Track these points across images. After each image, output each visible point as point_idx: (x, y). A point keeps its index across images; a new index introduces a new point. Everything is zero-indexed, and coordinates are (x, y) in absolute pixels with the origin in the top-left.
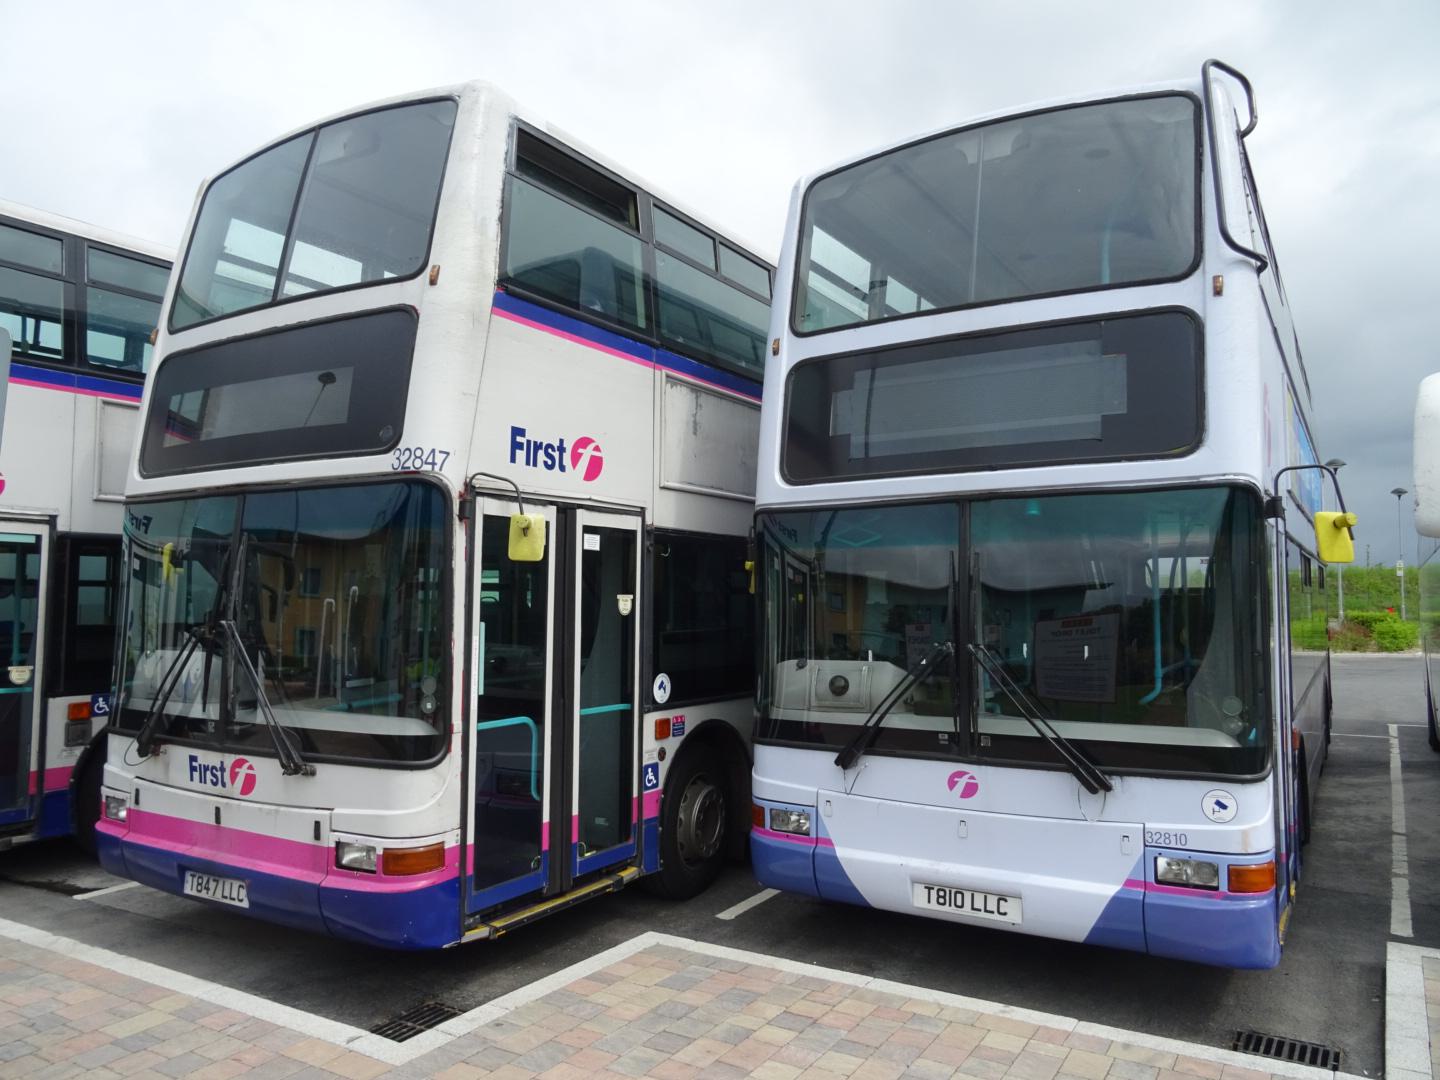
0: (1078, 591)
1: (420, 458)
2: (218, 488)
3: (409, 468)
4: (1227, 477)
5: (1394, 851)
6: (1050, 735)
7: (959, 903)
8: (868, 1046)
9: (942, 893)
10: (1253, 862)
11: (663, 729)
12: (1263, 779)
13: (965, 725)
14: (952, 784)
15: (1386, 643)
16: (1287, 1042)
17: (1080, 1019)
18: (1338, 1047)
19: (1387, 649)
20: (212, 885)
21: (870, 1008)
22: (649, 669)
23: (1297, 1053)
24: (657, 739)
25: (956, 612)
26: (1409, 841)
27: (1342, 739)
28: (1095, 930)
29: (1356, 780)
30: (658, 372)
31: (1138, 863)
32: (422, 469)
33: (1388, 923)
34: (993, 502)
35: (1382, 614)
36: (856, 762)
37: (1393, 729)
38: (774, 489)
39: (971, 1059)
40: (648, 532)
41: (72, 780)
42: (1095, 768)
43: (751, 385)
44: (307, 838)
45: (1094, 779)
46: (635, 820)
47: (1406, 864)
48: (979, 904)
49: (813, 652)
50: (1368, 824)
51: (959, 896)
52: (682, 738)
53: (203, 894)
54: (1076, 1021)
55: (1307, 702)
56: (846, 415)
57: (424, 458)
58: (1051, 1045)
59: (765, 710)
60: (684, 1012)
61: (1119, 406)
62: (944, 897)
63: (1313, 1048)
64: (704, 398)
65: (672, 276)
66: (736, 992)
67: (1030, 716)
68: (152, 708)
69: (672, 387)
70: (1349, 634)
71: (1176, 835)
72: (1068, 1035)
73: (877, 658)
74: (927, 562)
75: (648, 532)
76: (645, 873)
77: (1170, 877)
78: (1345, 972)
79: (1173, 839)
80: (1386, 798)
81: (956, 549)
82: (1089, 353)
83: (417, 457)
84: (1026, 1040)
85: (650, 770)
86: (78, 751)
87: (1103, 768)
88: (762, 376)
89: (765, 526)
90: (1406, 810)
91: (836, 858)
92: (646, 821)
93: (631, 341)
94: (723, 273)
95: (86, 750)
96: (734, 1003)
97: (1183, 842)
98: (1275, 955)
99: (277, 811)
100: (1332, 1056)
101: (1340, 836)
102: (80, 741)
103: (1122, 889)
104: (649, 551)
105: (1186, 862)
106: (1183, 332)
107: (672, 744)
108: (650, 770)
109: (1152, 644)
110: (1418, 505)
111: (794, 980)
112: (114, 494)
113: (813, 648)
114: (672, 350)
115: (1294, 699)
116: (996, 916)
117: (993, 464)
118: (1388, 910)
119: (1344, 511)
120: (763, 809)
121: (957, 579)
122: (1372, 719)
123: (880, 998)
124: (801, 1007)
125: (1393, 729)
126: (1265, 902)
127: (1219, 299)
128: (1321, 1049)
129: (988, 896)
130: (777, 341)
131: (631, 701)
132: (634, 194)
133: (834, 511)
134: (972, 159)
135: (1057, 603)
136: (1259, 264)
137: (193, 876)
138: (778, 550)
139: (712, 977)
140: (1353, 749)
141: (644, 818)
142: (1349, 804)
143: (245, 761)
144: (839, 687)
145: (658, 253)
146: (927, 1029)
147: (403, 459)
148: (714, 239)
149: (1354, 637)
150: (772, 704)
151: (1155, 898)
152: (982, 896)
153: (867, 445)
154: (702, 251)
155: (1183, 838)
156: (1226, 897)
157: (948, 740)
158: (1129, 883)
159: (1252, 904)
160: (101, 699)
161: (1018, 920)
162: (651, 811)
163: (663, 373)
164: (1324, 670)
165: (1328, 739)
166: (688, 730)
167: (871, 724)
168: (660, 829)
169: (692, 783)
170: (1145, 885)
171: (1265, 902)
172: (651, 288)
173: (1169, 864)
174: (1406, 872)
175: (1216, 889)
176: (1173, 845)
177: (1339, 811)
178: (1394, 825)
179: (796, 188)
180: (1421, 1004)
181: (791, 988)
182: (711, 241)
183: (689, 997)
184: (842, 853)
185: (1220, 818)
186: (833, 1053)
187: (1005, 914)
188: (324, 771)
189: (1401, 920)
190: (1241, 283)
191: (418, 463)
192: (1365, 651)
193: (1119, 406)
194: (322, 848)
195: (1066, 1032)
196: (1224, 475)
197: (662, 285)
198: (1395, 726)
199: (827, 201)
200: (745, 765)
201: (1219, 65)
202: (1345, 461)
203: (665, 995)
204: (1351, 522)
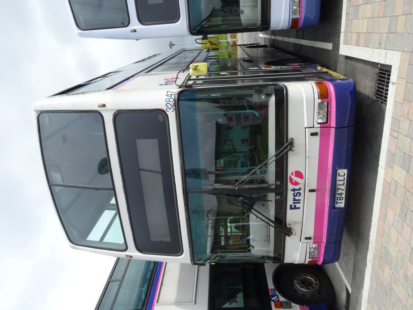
1: (169, 99)
2: (185, 205)
3: (173, 103)
10: (316, 90)
13: (271, 191)
20: (340, 192)
32: (174, 98)
41: (305, 306)
44: (317, 139)
53: (344, 196)
57: (169, 98)
59: (269, 258)
68: (273, 226)
83: (169, 101)
86: (293, 304)
95: (293, 302)
99: (308, 156)
102: (289, 304)
105: (319, 113)
112: (193, 299)
127: (106, 105)
137: (337, 203)
143: (290, 176)
147: (170, 107)
160: (272, 299)
167: (273, 225)
182: (110, 283)
187: (344, 174)
188: (291, 135)
191: (171, 100)
194: (321, 131)
200: (293, 267)
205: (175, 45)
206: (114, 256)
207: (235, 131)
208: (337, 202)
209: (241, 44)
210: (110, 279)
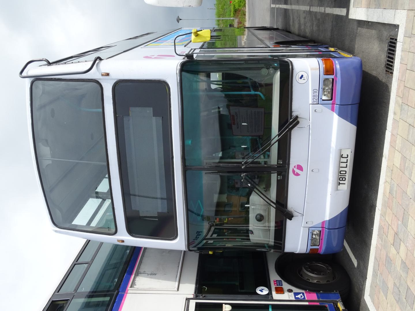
0: (221, 117)
4: (178, 73)
5: (316, 11)
6: (277, 138)
7: (344, 172)
8: (404, 214)
9: (341, 179)
10: (322, 66)
11: (280, 290)
12: (291, 62)
14: (298, 175)
15: (242, 5)
16: (388, 55)
17: (386, 129)
18: (388, 38)
19: (245, 4)
21: (389, 211)
22: (254, 297)
23: (392, 52)
24: (284, 293)
25: (229, 172)
26: (312, 6)
27: (277, 23)
28: (351, 122)
29: (291, 21)
30: (129, 292)
31: (325, 107)
33: (342, 16)
34: (186, 158)
35: (232, 5)
36: (290, 211)
37: (273, 6)
38: (179, 243)
39: (405, 173)
40: (196, 297)
42: (289, 121)
43: (136, 251)
45: (293, 123)
46: (318, 304)
47: (320, 8)
48: (344, 165)
49: (247, 225)
50: (307, 18)
51: (342, 172)
52: (283, 281)
54: (387, 131)
55: (263, 39)
56: (151, 208)
58: (397, 142)
59: (270, 247)
60: (397, 289)
61: (149, 111)
62: (342, 178)
63: (389, 46)
64: (141, 270)
65: (87, 286)
66: (387, 265)
67: (270, 145)
69: (136, 285)
70: (240, 16)
71: (314, 93)
72: (392, 135)
73: (248, 203)
74: (210, 182)
75: (196, 297)
76: (340, 299)
77: (329, 95)
78: (361, 32)
79: (315, 94)
80: (297, 11)
81: (204, 172)
82: (129, 121)
84: (396, 151)
85: (297, 297)
87: (289, 118)
88: (132, 247)
89: (195, 247)
90: (301, 5)
91: (329, 220)
92: (318, 299)
93: (115, 304)
94: (90, 260)
96: (391, 267)
97: (316, 90)
98: (356, 59)
100: (392, 40)
101: (312, 28)
103: (335, 112)
104: (205, 296)
105: (324, 89)
106: (121, 87)
107: (286, 286)
108: (297, 297)
109: (241, 95)
110: (190, 6)
111: (380, 239)
113: (245, 225)
114: (120, 284)
115: (262, 46)
116: (349, 158)
117: (171, 157)
118: (337, 15)
119: (192, 33)
120: (311, 249)
121: (217, 172)
122: (270, 12)
123: (384, 205)
124: (391, 238)
125: (273, 6)
126: (337, 62)
127: (110, 74)
128: (389, 44)
129: (341, 161)
130: (118, 241)
131: (268, 305)
132: (53, 301)
133: (188, 211)
134: (50, 162)
135: (226, 125)
136: (98, 60)
138: (205, 241)
139: (381, 274)
140: (280, 20)
141: (317, 299)
142: (300, 23)
144: (260, 218)
145: (78, 291)
146: (395, 189)
148: (75, 264)
149: (240, 15)
150: (268, 244)
151: (338, 100)
152: (341, 163)
153: (162, 199)
154: (80, 269)
155: (314, 90)
156: (336, 76)
157: (280, 176)
158: (333, 110)
159: (338, 66)
161: (350, 151)
162: (314, 296)
163: (130, 290)
164: (252, 30)
165: (277, 29)
166: (280, 279)
167: (275, 206)
168: (321, 292)
169: (302, 277)
170: (333, 104)
171: (337, 62)
172: (92, 294)
173: (325, 95)
174: (323, 8)
175: (333, 79)
176: (317, 94)
177: (302, 27)
178: (307, 10)
179: (56, 231)
180: (370, 10)
181: (383, 242)
182: (76, 265)
183: (390, 285)
184: (327, 218)
185: (307, 77)
186: (408, 228)
187: (348, 155)
189: (342, 12)
190: (105, 66)
192: (246, 11)
193: (149, 111)
195: (391, 135)
196: (177, 74)
197: (91, 289)
198: (272, 5)
199: (62, 217)
201: (22, 72)
202: (177, 16)
203: (390, 296)
204: (196, 31)
205: (182, 19)
206: (84, 238)
207: (238, 111)
208: (339, 182)
209: (249, 27)
210: (77, 262)
